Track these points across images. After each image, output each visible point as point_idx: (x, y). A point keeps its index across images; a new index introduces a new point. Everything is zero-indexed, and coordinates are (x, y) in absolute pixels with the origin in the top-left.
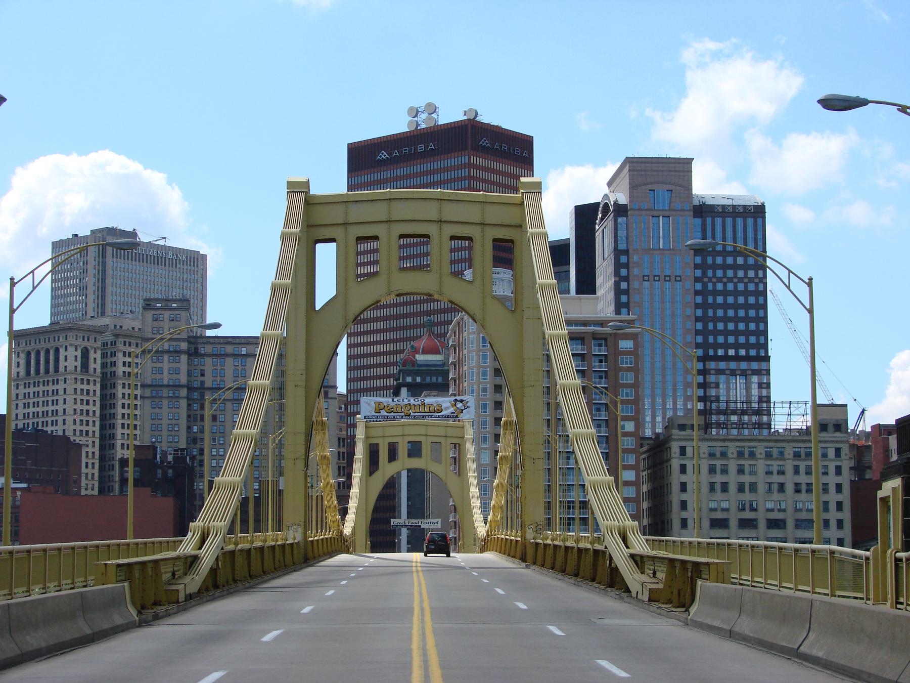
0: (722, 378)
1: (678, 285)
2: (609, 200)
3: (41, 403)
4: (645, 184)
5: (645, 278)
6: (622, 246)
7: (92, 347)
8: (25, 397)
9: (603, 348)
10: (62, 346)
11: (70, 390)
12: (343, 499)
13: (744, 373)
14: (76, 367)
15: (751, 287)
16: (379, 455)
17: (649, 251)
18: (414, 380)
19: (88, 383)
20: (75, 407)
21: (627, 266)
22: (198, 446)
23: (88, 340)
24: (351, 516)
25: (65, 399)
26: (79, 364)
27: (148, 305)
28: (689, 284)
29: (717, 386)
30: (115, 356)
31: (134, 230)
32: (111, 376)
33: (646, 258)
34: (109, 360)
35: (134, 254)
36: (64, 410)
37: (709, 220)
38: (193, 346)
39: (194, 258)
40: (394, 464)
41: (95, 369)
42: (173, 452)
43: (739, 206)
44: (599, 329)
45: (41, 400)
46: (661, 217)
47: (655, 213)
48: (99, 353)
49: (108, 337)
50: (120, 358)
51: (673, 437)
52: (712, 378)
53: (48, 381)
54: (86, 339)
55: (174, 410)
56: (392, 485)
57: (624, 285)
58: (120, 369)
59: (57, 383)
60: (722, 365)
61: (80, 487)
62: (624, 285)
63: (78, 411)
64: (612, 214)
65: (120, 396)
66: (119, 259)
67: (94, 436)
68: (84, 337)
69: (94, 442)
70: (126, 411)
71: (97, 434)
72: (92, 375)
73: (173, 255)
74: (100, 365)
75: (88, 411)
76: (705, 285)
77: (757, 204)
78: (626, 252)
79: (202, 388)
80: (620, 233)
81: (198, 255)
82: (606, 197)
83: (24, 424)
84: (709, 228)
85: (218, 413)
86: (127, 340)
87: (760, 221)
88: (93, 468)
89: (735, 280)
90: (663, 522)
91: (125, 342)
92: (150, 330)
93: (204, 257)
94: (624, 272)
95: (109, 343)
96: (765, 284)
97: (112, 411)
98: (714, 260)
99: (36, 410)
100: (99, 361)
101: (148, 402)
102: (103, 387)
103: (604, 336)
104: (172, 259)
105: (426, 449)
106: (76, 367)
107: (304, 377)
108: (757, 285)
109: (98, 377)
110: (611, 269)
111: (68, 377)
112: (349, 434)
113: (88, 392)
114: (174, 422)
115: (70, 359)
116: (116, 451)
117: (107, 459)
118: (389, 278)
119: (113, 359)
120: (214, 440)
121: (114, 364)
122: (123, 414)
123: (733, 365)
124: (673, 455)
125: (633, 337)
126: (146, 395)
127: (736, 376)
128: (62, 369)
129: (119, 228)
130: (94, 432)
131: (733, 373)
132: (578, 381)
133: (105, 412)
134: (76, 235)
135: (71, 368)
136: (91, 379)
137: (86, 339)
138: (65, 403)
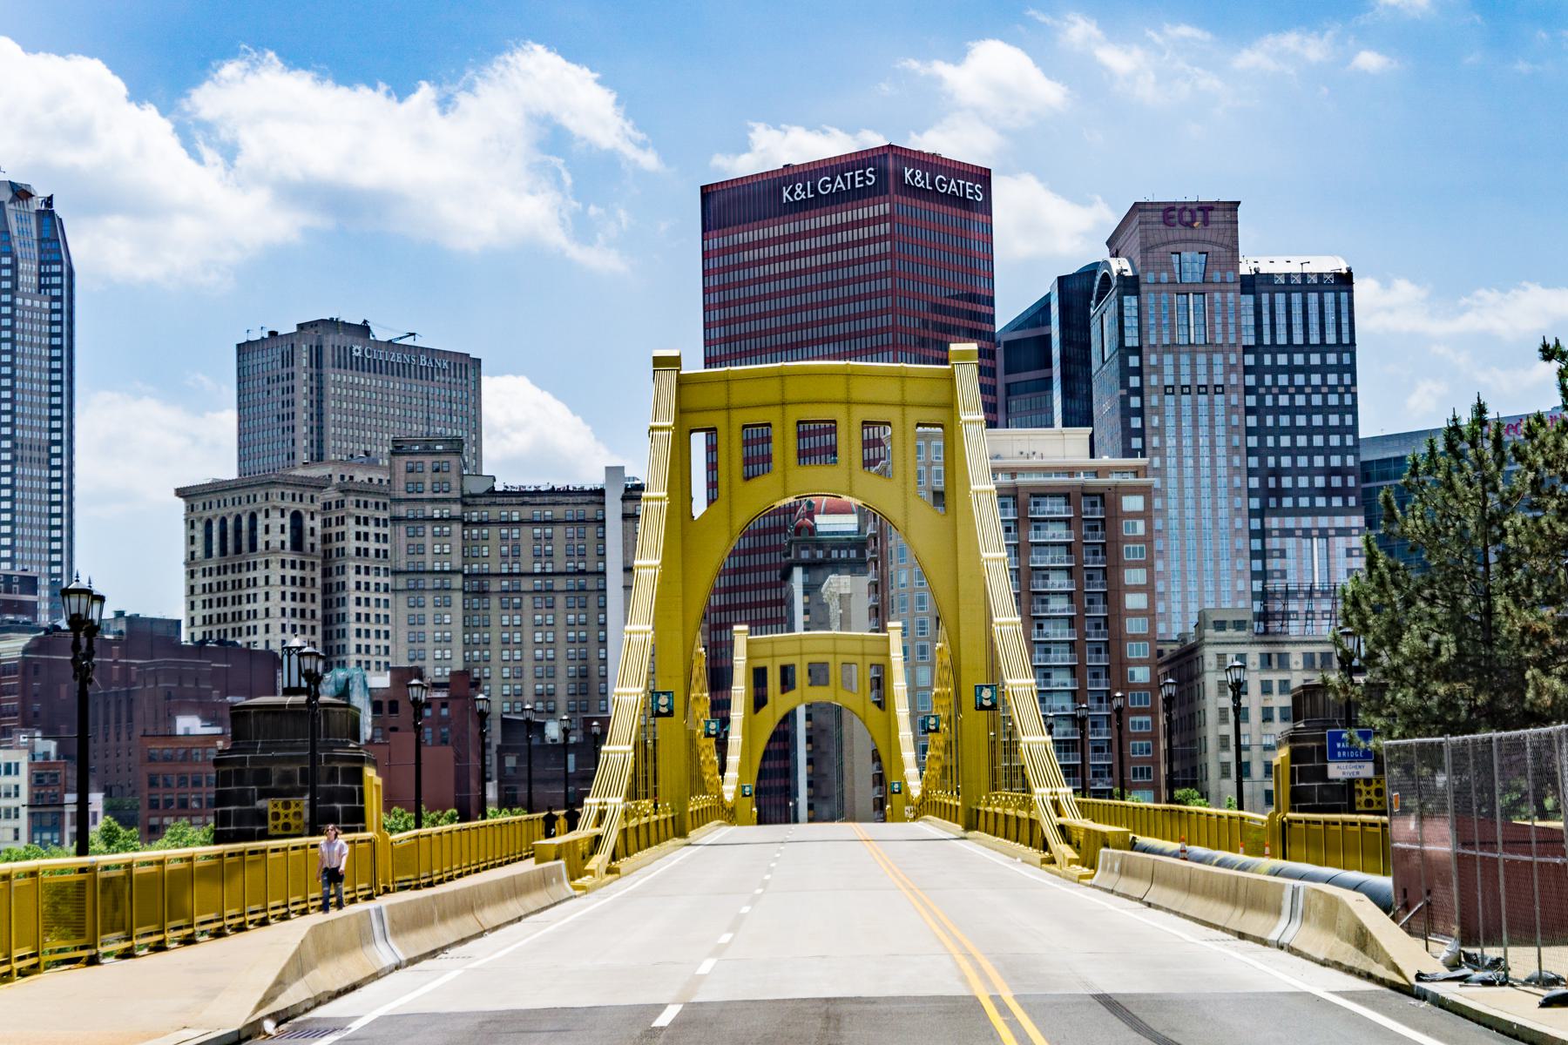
0: (1290, 543)
3: (230, 600)
4: (1164, 244)
5: (1167, 390)
7: (307, 511)
8: (204, 591)
9: (1098, 508)
10: (260, 510)
11: (275, 579)
12: (722, 746)
13: (1323, 533)
14: (283, 543)
15: (1333, 400)
20: (283, 604)
23: (301, 500)
24: (732, 774)
25: (267, 594)
26: (287, 537)
27: (398, 449)
29: (1283, 554)
30: (343, 523)
31: (365, 322)
33: (1168, 359)
34: (334, 530)
36: (267, 610)
37: (1265, 298)
40: (790, 695)
41: (312, 545)
43: (1312, 274)
44: (1092, 480)
45: (229, 595)
46: (1191, 295)
48: (318, 519)
50: (351, 527)
51: (1207, 640)
52: (1274, 543)
53: (211, 569)
54: (297, 498)
57: (1135, 402)
58: (351, 545)
59: (255, 568)
60: (1290, 522)
62: (1135, 402)
63: (288, 611)
68: (294, 495)
70: (363, 610)
76: (1261, 399)
83: (204, 633)
86: (362, 499)
87: (1344, 296)
89: (1308, 390)
90: (1194, 769)
91: (358, 502)
92: (403, 486)
98: (1274, 359)
99: (222, 610)
101: (402, 598)
103: (1100, 491)
105: (834, 673)
106: (283, 543)
108: (1341, 396)
111: (271, 558)
115: (274, 531)
118: (785, 476)
123: (1306, 522)
124: (1207, 668)
125: (1146, 491)
126: (399, 587)
128: (261, 545)
131: (1307, 533)
133: (330, 611)
134: (273, 334)
135: (274, 544)
137: (297, 498)
138: (267, 599)
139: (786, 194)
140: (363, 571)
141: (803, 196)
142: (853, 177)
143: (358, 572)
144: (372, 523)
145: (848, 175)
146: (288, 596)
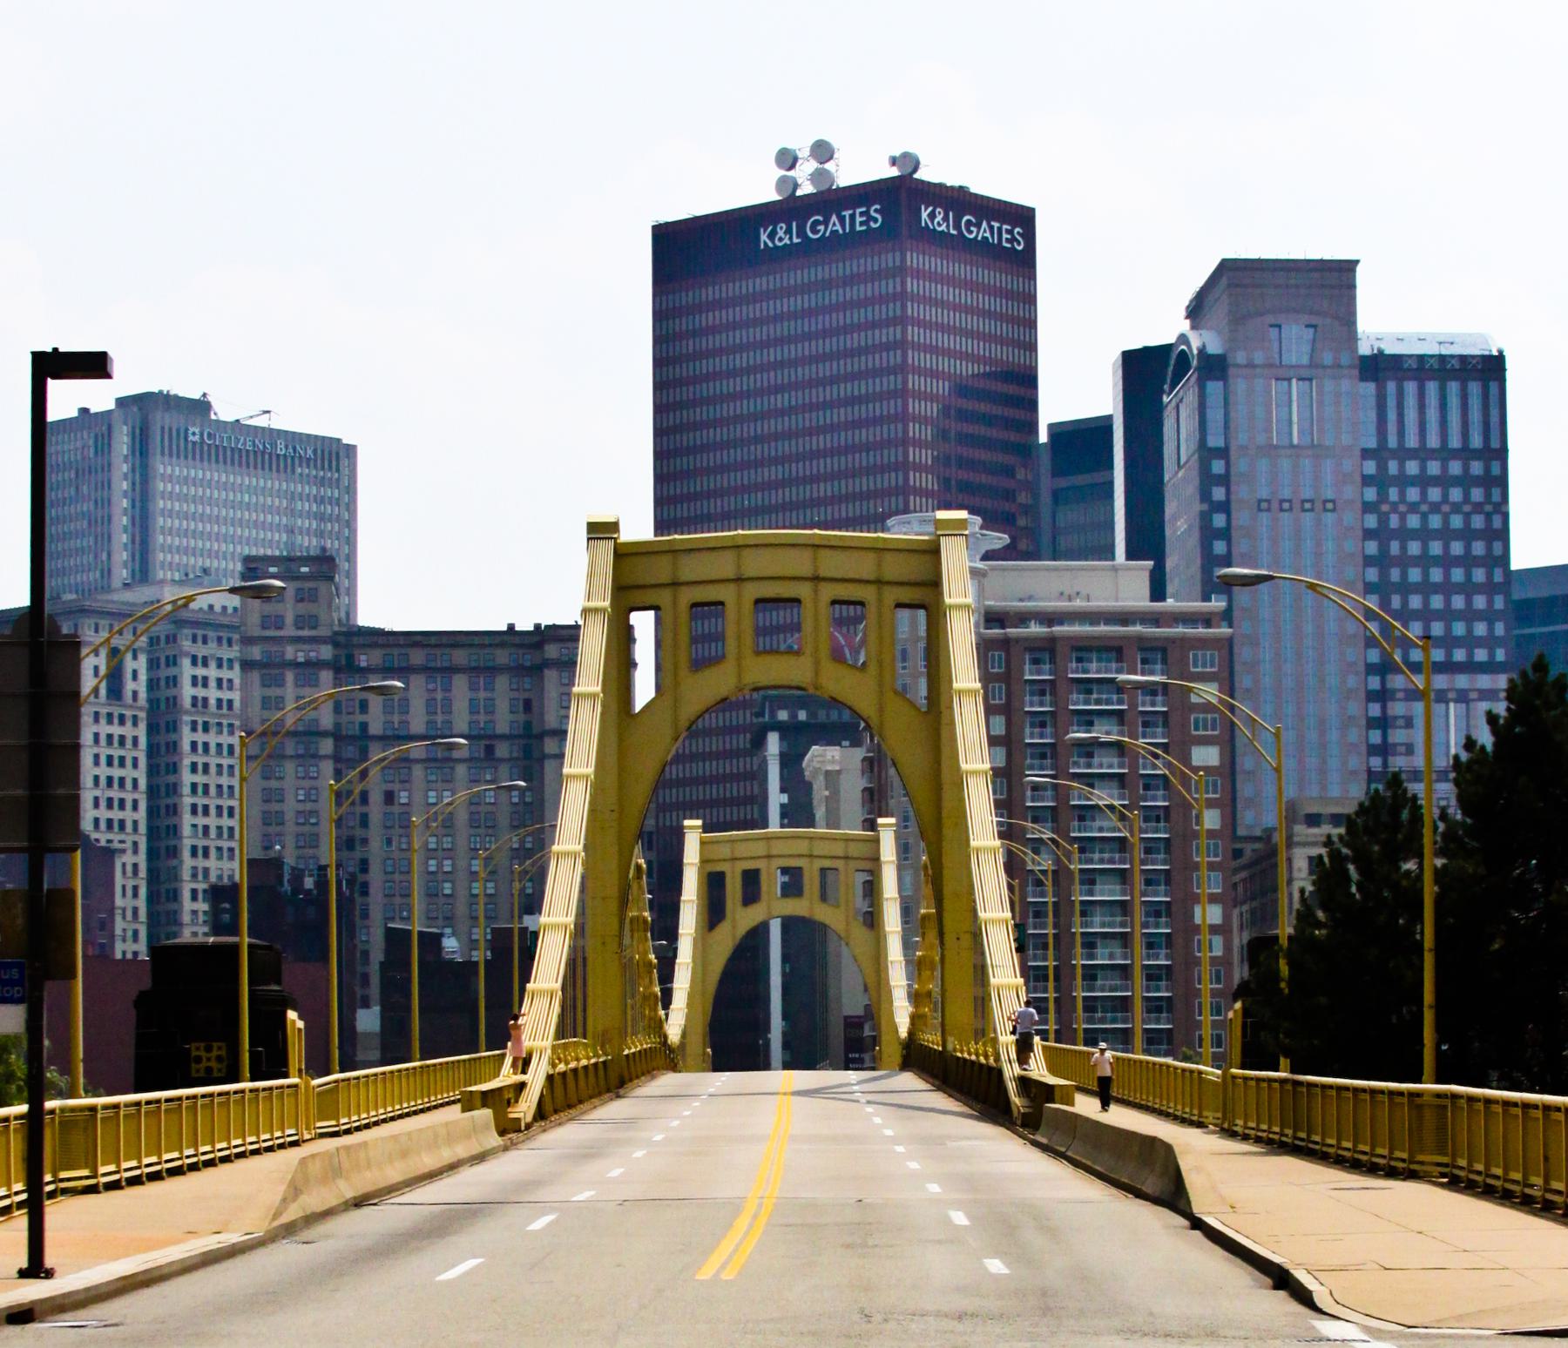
0: (1418, 708)
1: (1329, 518)
2: (1189, 346)
6: (1215, 441)
13: (1463, 697)
16: (695, 220)
17: (1270, 450)
18: (794, 716)
19: (206, 728)
21: (1225, 480)
22: (358, 854)
28: (1350, 517)
29: (1409, 723)
30: (175, 664)
31: (204, 395)
32: (168, 706)
34: (164, 673)
35: (206, 448)
37: (1391, 387)
38: (343, 652)
39: (330, 454)
41: (135, 694)
42: (315, 872)
47: (1281, 372)
49: (162, 629)
50: (187, 670)
52: (1397, 708)
55: (307, 783)
56: (752, 947)
57: (1219, 520)
58: (187, 692)
61: (112, 937)
64: (1196, 375)
65: (186, 747)
66: (174, 459)
67: (135, 829)
69: (135, 844)
70: (200, 779)
71: (143, 828)
72: (131, 707)
73: (286, 447)
74: (145, 684)
75: (122, 781)
77: (1487, 353)
78: (1223, 453)
79: (363, 736)
80: (1210, 414)
81: (338, 447)
82: (1183, 338)
84: (1391, 402)
85: (396, 787)
86: (200, 633)
87: (1493, 387)
88: (135, 895)
93: (351, 450)
94: (1218, 494)
95: (163, 638)
96: (1506, 516)
97: (171, 779)
100: (143, 677)
102: (152, 729)
103: (1160, 645)
104: (285, 455)
105: (811, 882)
107: (615, 815)
108: (1488, 516)
109: (141, 709)
110: (1191, 489)
112: (661, 824)
113: (122, 739)
114: (309, 806)
116: (181, 862)
117: (162, 878)
119: (172, 671)
120: (389, 842)
121: (174, 681)
122: (194, 786)
127: (1447, 703)
129: (172, 393)
130: (135, 823)
132: (998, 843)
136: (128, 713)
139: (764, 237)
140: (200, 728)
141: (787, 241)
142: (853, 217)
143: (194, 729)
144: (213, 664)
145: (847, 213)
146: (103, 760)
